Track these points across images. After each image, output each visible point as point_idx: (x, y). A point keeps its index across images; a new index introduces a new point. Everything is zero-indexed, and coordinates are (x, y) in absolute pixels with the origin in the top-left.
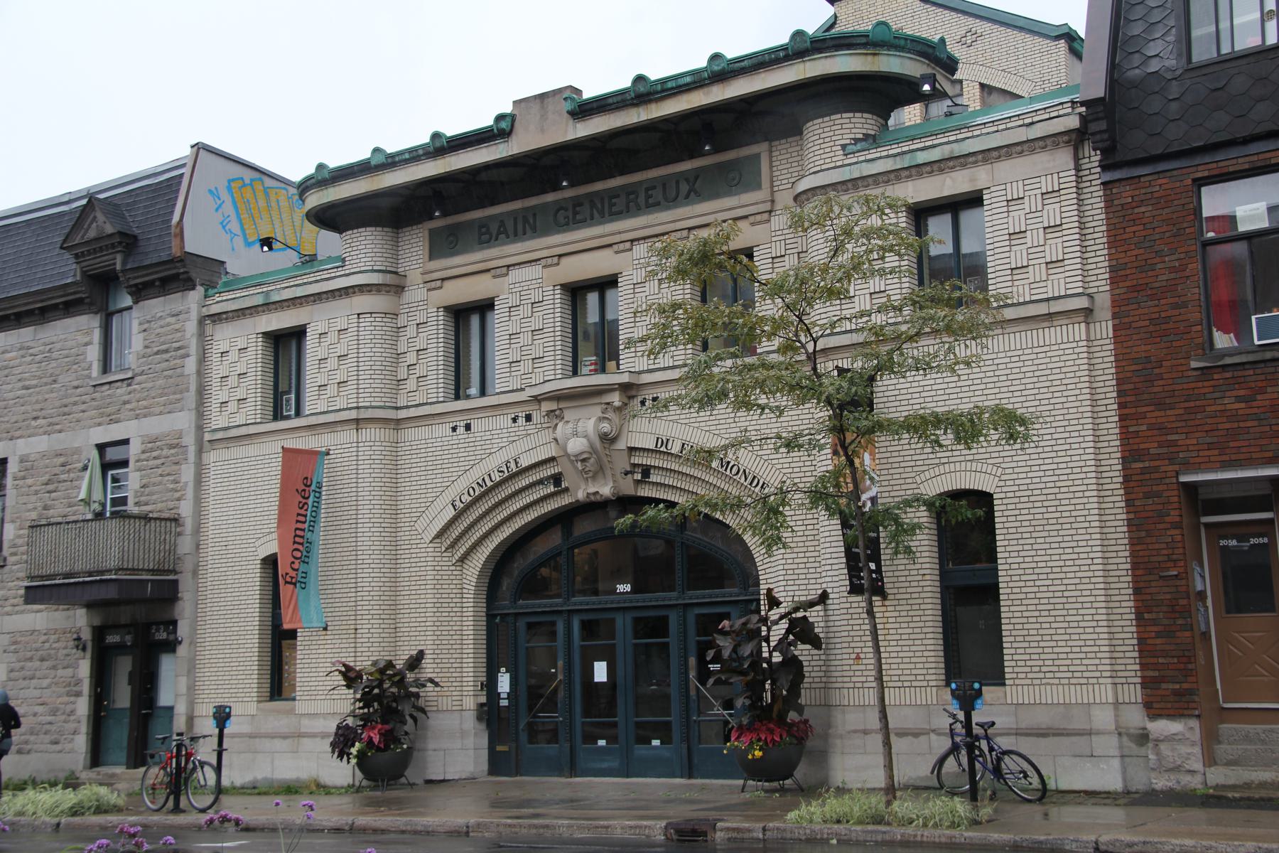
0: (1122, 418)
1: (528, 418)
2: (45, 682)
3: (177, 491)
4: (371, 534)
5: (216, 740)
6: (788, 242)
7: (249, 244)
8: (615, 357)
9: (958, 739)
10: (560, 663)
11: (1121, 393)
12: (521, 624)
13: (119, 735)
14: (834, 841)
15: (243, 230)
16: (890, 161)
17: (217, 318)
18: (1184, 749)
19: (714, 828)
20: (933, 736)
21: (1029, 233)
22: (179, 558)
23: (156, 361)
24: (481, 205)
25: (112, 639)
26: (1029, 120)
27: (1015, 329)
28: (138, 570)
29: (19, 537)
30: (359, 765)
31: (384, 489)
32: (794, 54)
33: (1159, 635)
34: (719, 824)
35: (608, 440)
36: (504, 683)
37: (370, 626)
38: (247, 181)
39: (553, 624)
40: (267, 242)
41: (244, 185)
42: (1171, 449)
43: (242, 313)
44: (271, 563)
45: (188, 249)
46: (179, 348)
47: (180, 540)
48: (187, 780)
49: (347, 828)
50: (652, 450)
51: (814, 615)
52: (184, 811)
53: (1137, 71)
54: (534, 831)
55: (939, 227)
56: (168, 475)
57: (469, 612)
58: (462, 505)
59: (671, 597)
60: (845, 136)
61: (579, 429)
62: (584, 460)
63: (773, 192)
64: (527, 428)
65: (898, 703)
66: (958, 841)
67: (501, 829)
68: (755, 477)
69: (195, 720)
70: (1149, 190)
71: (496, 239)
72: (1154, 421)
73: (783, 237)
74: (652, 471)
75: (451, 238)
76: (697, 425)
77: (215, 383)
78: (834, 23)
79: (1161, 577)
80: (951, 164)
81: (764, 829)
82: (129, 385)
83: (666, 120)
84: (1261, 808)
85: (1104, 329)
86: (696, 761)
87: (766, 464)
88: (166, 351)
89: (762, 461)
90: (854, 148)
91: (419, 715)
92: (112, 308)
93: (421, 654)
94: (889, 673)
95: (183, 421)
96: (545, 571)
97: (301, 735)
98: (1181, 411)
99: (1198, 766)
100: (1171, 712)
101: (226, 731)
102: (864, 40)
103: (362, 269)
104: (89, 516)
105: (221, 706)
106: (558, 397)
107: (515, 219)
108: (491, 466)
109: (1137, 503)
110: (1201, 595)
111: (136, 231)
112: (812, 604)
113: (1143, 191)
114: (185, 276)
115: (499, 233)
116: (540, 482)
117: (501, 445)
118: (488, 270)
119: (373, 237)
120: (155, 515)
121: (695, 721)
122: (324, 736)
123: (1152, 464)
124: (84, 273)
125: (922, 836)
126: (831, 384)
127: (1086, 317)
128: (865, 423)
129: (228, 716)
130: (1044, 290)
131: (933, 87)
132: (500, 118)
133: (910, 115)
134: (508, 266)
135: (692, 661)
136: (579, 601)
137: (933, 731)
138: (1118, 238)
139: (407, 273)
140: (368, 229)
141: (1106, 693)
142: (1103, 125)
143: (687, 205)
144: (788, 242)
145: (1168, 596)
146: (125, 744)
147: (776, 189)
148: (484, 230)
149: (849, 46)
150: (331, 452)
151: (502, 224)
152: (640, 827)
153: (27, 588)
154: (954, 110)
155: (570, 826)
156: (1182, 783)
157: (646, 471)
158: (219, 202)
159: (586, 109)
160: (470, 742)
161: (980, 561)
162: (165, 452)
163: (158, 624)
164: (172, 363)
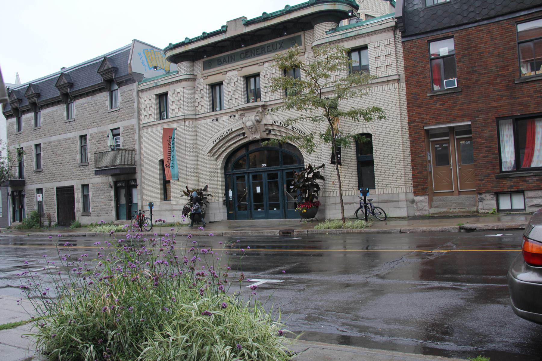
0: (408, 111)
1: (235, 116)
2: (103, 197)
5: (150, 212)
7: (150, 69)
8: (260, 97)
9: (362, 204)
10: (247, 188)
11: (408, 104)
12: (235, 177)
13: (123, 211)
15: (148, 65)
16: (340, 36)
17: (142, 91)
18: (424, 204)
19: (293, 231)
20: (355, 204)
24: (218, 54)
25: (119, 185)
26: (380, 24)
29: (92, 157)
30: (190, 218)
33: (418, 173)
34: (295, 230)
35: (258, 122)
36: (230, 194)
38: (149, 50)
39: (244, 177)
40: (155, 67)
41: (148, 51)
43: (149, 89)
44: (162, 161)
45: (133, 71)
47: (136, 156)
48: (143, 222)
51: (321, 170)
53: (411, 9)
55: (355, 56)
57: (219, 174)
59: (278, 167)
62: (251, 128)
63: (305, 46)
77: (143, 110)
80: (358, 36)
81: (308, 231)
84: (443, 218)
85: (403, 85)
86: (287, 214)
88: (128, 101)
90: (329, 32)
91: (207, 204)
92: (112, 90)
93: (207, 186)
94: (343, 187)
95: (134, 121)
96: (241, 162)
97: (173, 210)
99: (427, 208)
101: (152, 209)
104: (110, 150)
106: (243, 110)
108: (224, 131)
109: (413, 135)
110: (430, 161)
111: (118, 67)
112: (320, 167)
115: (224, 61)
116: (239, 135)
118: (221, 73)
122: (180, 210)
123: (417, 124)
124: (104, 80)
126: (328, 103)
127: (398, 81)
128: (335, 113)
129: (153, 205)
131: (352, 14)
132: (223, 27)
133: (344, 23)
135: (285, 186)
136: (251, 170)
142: (402, 25)
143: (279, 51)
146: (125, 214)
151: (224, 59)
153: (95, 171)
154: (358, 21)
155: (252, 232)
157: (270, 131)
159: (248, 23)
160: (222, 211)
161: (368, 154)
163: (131, 180)
164: (130, 105)
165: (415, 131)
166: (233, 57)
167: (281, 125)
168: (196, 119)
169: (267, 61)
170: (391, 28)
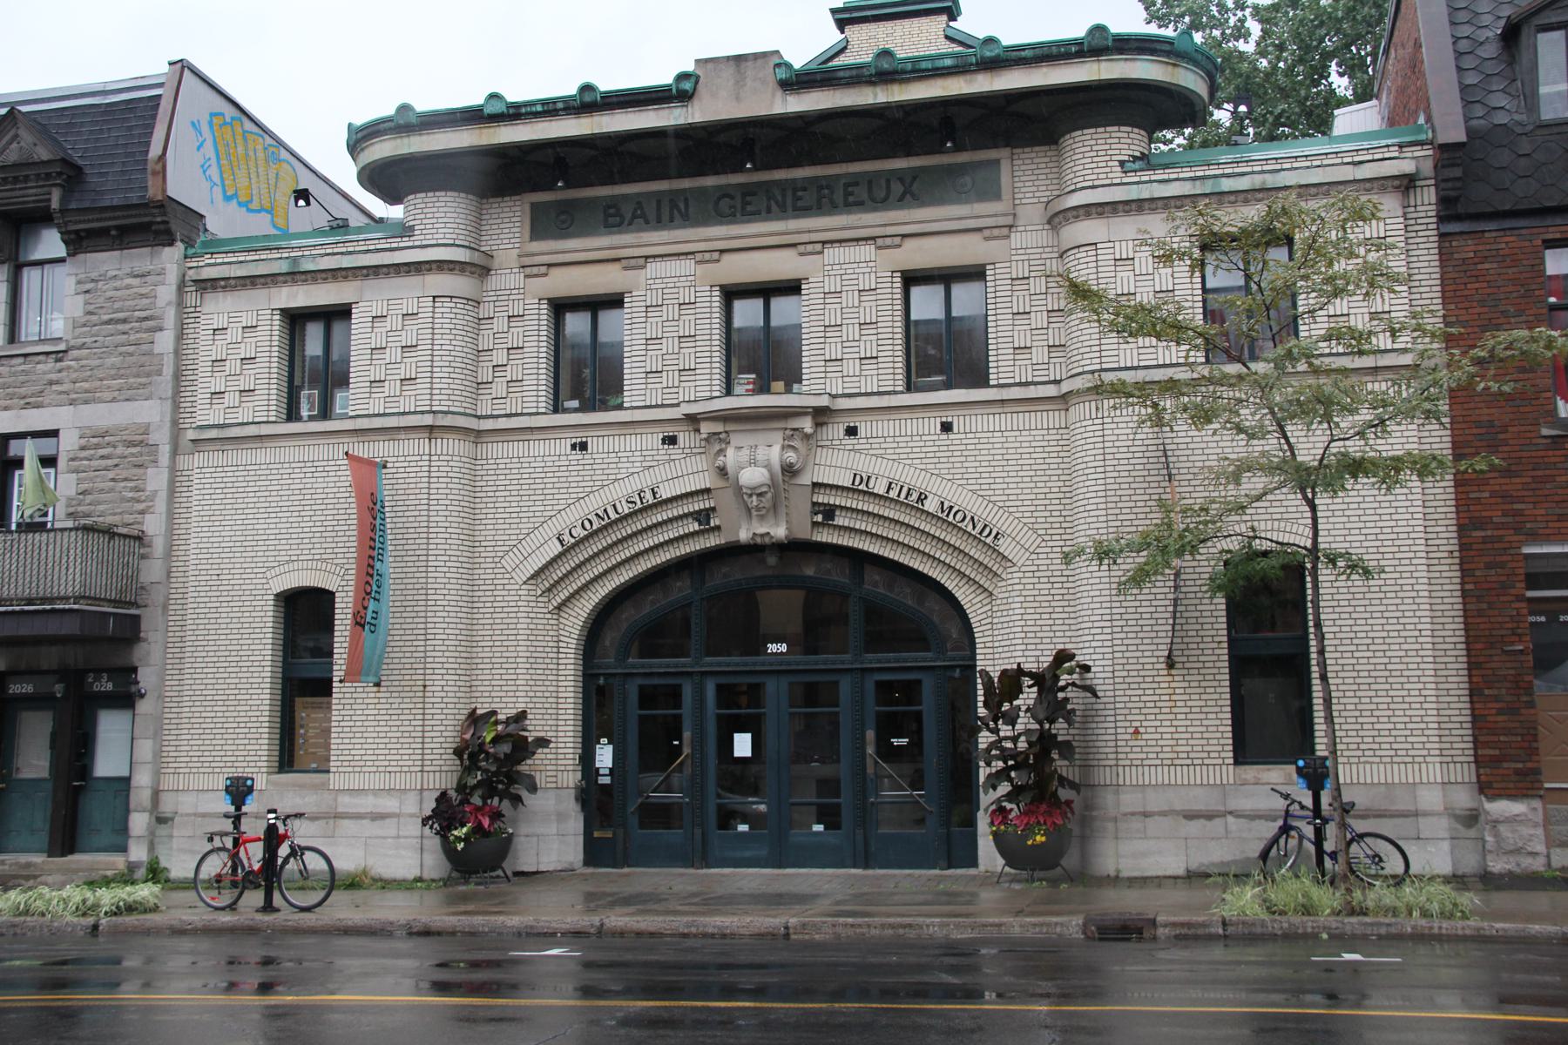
3: (138, 501)
4: (446, 569)
6: (1032, 263)
14: (1325, 936)
15: (223, 180)
16: (1188, 185)
18: (1526, 831)
20: (1230, 819)
21: (388, 350)
22: (142, 588)
23: (104, 333)
27: (413, 436)
28: (100, 599)
31: (462, 515)
32: (1089, 51)
33: (1500, 712)
35: (789, 471)
36: (605, 756)
37: (444, 683)
38: (228, 120)
42: (1517, 519)
43: (251, 281)
46: (146, 319)
49: (592, 931)
50: (848, 489)
52: (278, 910)
54: (890, 932)
56: (126, 479)
58: (573, 541)
59: (846, 660)
60: (1123, 152)
61: (759, 457)
62: (760, 495)
64: (669, 452)
65: (1186, 782)
66: (1488, 933)
67: (839, 930)
68: (986, 526)
69: (161, 794)
70: (1494, 247)
71: (630, 224)
72: (1497, 488)
73: (1026, 257)
74: (837, 513)
75: (563, 217)
76: (909, 462)
77: (203, 367)
78: (845, 48)
79: (1503, 651)
80: (1260, 196)
82: (60, 360)
83: (902, 106)
87: (1001, 511)
88: (124, 321)
89: (996, 508)
97: (338, 816)
98: (1529, 480)
99: (1540, 848)
100: (1513, 792)
102: (1167, 47)
103: (440, 242)
105: (238, 778)
107: (659, 202)
108: (619, 494)
113: (1488, 247)
114: (162, 227)
115: (634, 217)
116: (685, 516)
117: (631, 470)
119: (456, 205)
120: (124, 531)
121: (873, 803)
123: (1495, 533)
125: (1440, 928)
129: (250, 790)
130: (366, 406)
132: (683, 76)
134: (647, 257)
135: (870, 735)
137: (1231, 813)
138: (1458, 293)
139: (494, 253)
140: (449, 193)
141: (1434, 772)
143: (901, 208)
144: (1032, 263)
145: (1512, 672)
147: (1017, 202)
148: (612, 211)
149: (1153, 52)
150: (389, 465)
152: (1049, 925)
155: (942, 925)
156: (1523, 866)
157: (829, 512)
158: (201, 139)
162: (120, 450)
165: (1487, 559)
166: (682, 206)
167: (893, 494)
168: (478, 436)
169: (857, 240)
170: (1397, 183)
